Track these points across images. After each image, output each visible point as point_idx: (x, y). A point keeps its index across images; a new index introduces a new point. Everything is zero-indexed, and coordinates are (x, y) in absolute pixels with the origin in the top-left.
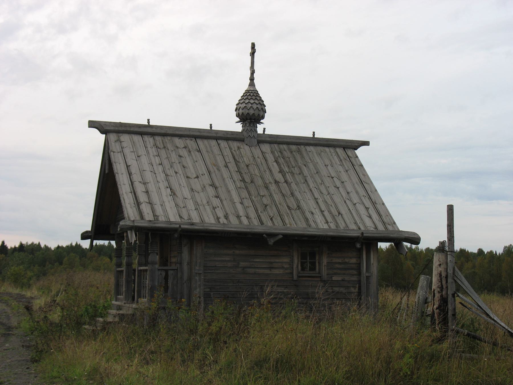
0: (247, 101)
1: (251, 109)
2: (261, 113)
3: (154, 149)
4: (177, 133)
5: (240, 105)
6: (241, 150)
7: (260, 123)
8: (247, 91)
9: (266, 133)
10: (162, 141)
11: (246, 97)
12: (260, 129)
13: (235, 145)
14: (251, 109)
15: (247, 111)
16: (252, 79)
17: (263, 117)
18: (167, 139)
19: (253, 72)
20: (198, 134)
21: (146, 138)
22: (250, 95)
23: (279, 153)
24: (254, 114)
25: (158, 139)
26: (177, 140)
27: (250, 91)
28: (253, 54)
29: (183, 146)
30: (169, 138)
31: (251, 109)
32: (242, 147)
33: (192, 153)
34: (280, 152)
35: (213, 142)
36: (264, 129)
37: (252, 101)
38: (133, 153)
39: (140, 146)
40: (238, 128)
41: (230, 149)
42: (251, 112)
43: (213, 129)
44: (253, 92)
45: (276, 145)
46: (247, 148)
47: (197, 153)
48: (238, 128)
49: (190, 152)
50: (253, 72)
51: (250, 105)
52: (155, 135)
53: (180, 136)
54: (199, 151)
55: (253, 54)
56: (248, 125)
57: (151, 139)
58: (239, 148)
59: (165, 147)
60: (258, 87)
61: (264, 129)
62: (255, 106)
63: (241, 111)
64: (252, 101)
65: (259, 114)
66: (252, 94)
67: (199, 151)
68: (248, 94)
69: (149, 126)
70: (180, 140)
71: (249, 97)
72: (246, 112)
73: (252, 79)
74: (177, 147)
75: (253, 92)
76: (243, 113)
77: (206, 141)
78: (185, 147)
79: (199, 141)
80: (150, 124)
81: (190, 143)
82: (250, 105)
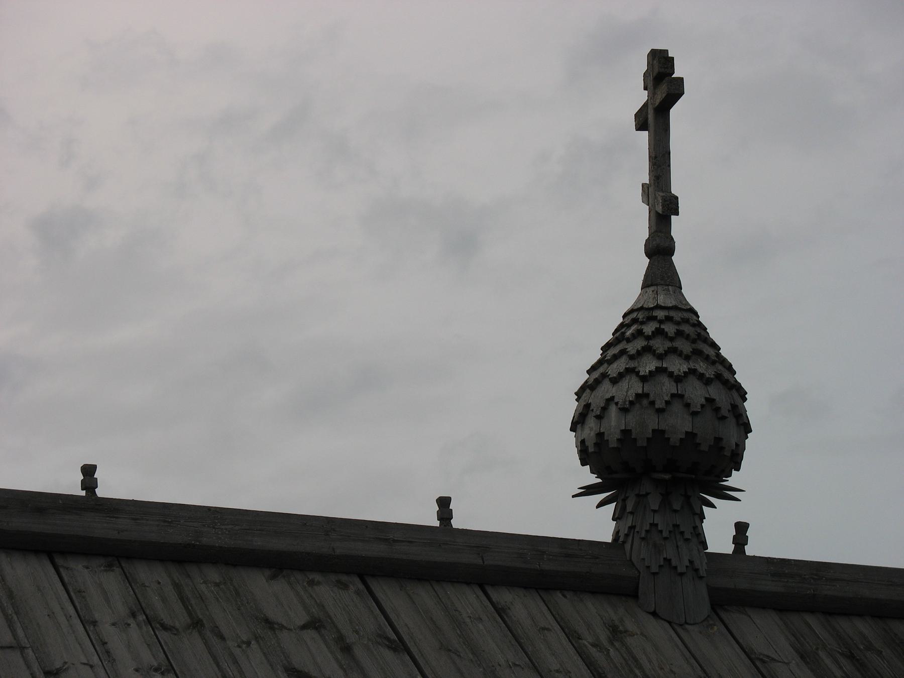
0: (648, 365)
1: (677, 407)
2: (730, 433)
3: (134, 632)
4: (258, 542)
5: (606, 390)
6: (629, 640)
7: (724, 493)
8: (635, 318)
9: (750, 550)
10: (177, 586)
11: (639, 344)
12: (717, 528)
13: (591, 614)
14: (665, 407)
15: (652, 422)
16: (660, 249)
17: (735, 460)
18: (206, 580)
19: (663, 205)
20: (376, 550)
21: (81, 572)
22: (659, 332)
23: (843, 661)
24: (691, 435)
25: (152, 576)
26: (260, 587)
27: (661, 314)
28: (655, 118)
29: (302, 618)
30: (213, 574)
31: (665, 407)
32: (630, 625)
33: (358, 652)
34: (851, 657)
35: (468, 601)
36: (741, 529)
37: (677, 366)
38: (16, 656)
39: (52, 615)
40: (596, 523)
41: (573, 636)
42: (679, 423)
43: (456, 523)
44: (677, 316)
45: (813, 621)
46: (657, 630)
47: (388, 654)
48: (596, 523)
49: (347, 649)
50: (663, 205)
51: (667, 387)
52: (63, 553)
53: (279, 564)
54: (399, 646)
55: (655, 118)
56: (654, 502)
57: (112, 581)
58: (616, 632)
59: (197, 624)
60: (696, 293)
61: (741, 529)
62: (696, 392)
63: (614, 422)
64: (677, 366)
65: (718, 440)
66: (670, 329)
67: (399, 646)
68: (648, 329)
69: (89, 502)
70: (279, 586)
71: (660, 345)
72: (645, 423)
73: (660, 249)
74: (269, 624)
75: (677, 316)
76: (626, 432)
77: (424, 594)
78: (314, 624)
79: (391, 595)
80: (101, 492)
81: (339, 600)
82: (667, 387)
